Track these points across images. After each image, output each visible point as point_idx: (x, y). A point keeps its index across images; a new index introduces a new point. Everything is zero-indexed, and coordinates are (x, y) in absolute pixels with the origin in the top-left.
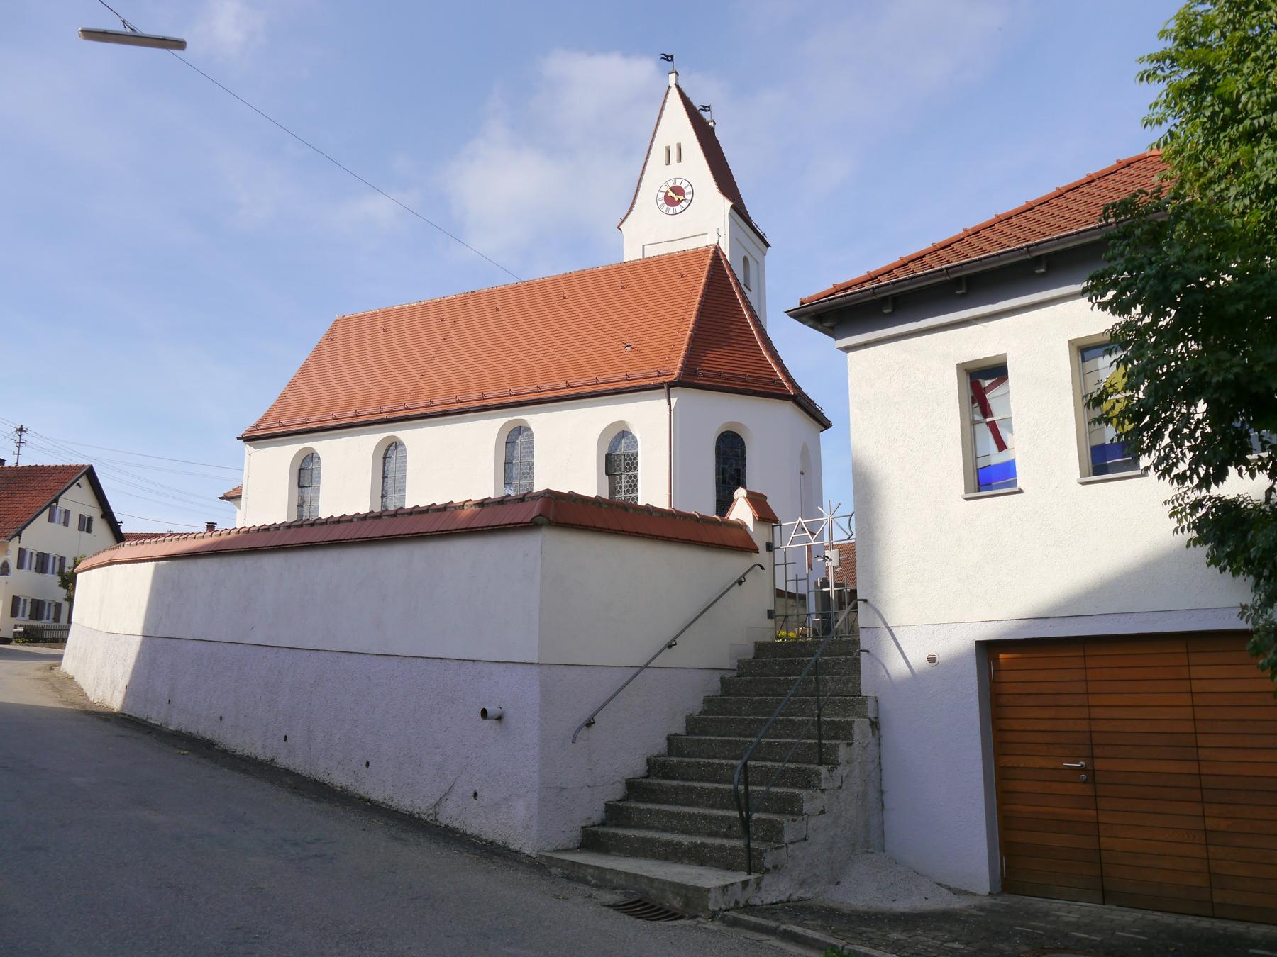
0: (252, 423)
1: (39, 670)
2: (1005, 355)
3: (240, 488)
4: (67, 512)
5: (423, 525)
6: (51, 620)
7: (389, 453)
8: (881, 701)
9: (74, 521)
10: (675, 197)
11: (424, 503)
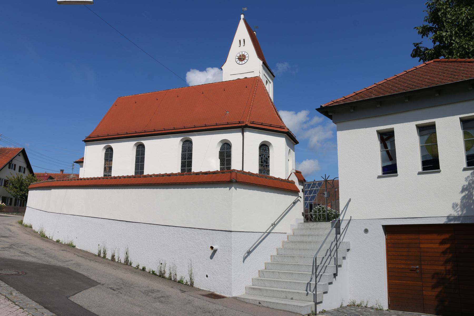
0: (88, 135)
1: (442, 243)
2: (393, 128)
3: (83, 159)
4: (15, 165)
5: (201, 179)
6: (19, 206)
7: (141, 150)
8: (321, 304)
9: (17, 168)
10: (242, 58)
11: (151, 173)
